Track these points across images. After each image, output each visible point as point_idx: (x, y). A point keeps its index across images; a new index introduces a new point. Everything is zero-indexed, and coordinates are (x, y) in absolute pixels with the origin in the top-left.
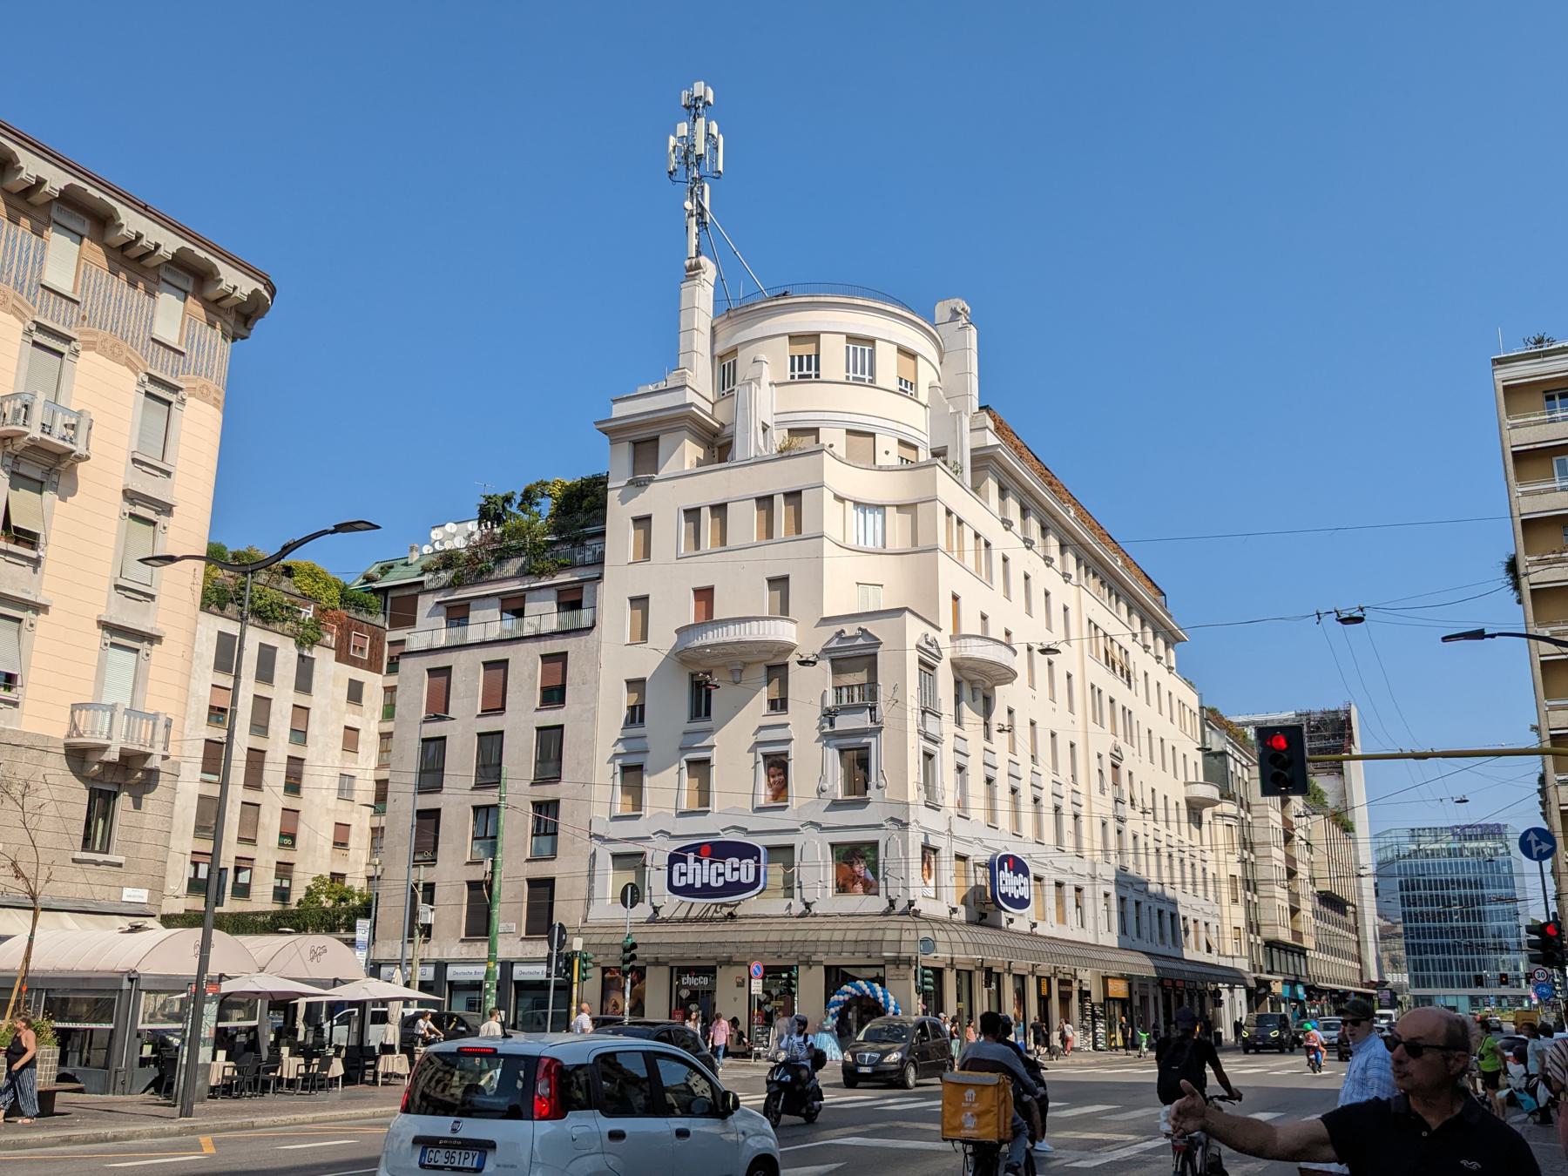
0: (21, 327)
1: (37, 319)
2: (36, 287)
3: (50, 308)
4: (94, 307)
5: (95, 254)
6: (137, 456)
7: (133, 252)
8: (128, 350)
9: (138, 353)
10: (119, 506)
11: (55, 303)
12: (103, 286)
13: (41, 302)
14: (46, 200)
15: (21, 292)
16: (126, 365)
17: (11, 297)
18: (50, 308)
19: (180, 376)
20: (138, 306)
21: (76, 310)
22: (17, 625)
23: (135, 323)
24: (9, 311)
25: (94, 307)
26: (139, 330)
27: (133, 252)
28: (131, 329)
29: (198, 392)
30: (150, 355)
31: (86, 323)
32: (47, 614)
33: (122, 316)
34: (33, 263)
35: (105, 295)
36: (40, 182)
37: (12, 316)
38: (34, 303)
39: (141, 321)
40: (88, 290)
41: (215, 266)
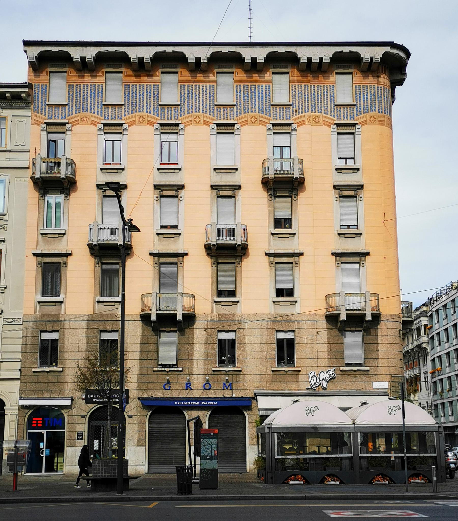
0: (265, 129)
1: (271, 122)
2: (269, 107)
3: (278, 114)
4: (300, 103)
5: (357, 76)
6: (337, 167)
7: (315, 67)
8: (323, 116)
9: (329, 116)
10: (333, 194)
11: (280, 110)
12: (303, 92)
13: (273, 113)
14: (367, 66)
15: (263, 113)
16: (324, 124)
17: (258, 118)
18: (278, 114)
19: (356, 118)
20: (324, 93)
21: (291, 109)
22: (292, 264)
23: (324, 101)
24: (258, 124)
25: (300, 103)
26: (327, 104)
27: (315, 67)
28: (323, 105)
29: (193, 122)
30: (336, 114)
31: (297, 113)
32: (370, 255)
33: (316, 101)
34: (266, 97)
35: (305, 96)
36: (310, 59)
37: (260, 126)
38: (270, 116)
39: (327, 99)
40: (295, 97)
41: (125, 53)
